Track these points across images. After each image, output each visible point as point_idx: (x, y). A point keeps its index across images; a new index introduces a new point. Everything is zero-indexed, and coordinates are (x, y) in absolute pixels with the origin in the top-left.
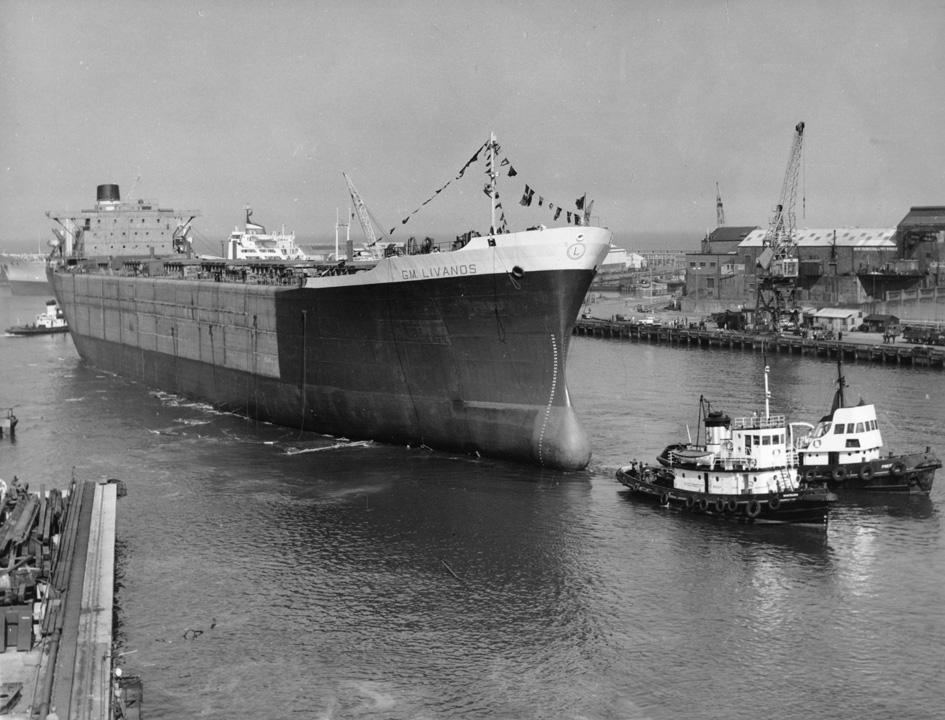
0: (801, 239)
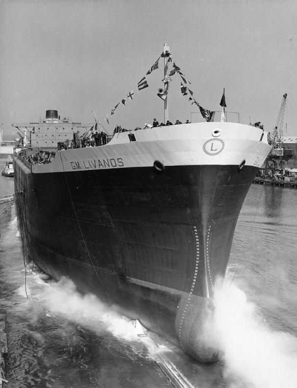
0: (285, 140)
